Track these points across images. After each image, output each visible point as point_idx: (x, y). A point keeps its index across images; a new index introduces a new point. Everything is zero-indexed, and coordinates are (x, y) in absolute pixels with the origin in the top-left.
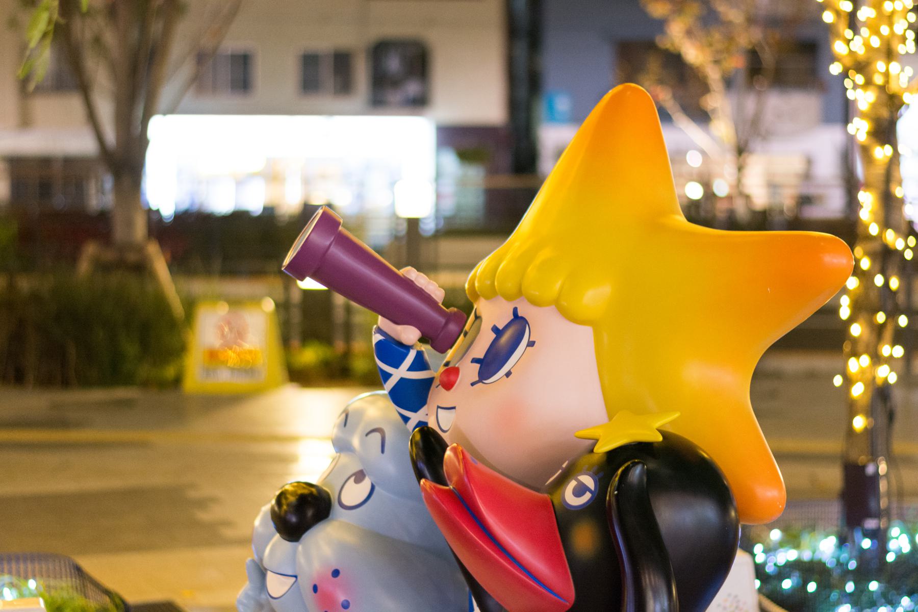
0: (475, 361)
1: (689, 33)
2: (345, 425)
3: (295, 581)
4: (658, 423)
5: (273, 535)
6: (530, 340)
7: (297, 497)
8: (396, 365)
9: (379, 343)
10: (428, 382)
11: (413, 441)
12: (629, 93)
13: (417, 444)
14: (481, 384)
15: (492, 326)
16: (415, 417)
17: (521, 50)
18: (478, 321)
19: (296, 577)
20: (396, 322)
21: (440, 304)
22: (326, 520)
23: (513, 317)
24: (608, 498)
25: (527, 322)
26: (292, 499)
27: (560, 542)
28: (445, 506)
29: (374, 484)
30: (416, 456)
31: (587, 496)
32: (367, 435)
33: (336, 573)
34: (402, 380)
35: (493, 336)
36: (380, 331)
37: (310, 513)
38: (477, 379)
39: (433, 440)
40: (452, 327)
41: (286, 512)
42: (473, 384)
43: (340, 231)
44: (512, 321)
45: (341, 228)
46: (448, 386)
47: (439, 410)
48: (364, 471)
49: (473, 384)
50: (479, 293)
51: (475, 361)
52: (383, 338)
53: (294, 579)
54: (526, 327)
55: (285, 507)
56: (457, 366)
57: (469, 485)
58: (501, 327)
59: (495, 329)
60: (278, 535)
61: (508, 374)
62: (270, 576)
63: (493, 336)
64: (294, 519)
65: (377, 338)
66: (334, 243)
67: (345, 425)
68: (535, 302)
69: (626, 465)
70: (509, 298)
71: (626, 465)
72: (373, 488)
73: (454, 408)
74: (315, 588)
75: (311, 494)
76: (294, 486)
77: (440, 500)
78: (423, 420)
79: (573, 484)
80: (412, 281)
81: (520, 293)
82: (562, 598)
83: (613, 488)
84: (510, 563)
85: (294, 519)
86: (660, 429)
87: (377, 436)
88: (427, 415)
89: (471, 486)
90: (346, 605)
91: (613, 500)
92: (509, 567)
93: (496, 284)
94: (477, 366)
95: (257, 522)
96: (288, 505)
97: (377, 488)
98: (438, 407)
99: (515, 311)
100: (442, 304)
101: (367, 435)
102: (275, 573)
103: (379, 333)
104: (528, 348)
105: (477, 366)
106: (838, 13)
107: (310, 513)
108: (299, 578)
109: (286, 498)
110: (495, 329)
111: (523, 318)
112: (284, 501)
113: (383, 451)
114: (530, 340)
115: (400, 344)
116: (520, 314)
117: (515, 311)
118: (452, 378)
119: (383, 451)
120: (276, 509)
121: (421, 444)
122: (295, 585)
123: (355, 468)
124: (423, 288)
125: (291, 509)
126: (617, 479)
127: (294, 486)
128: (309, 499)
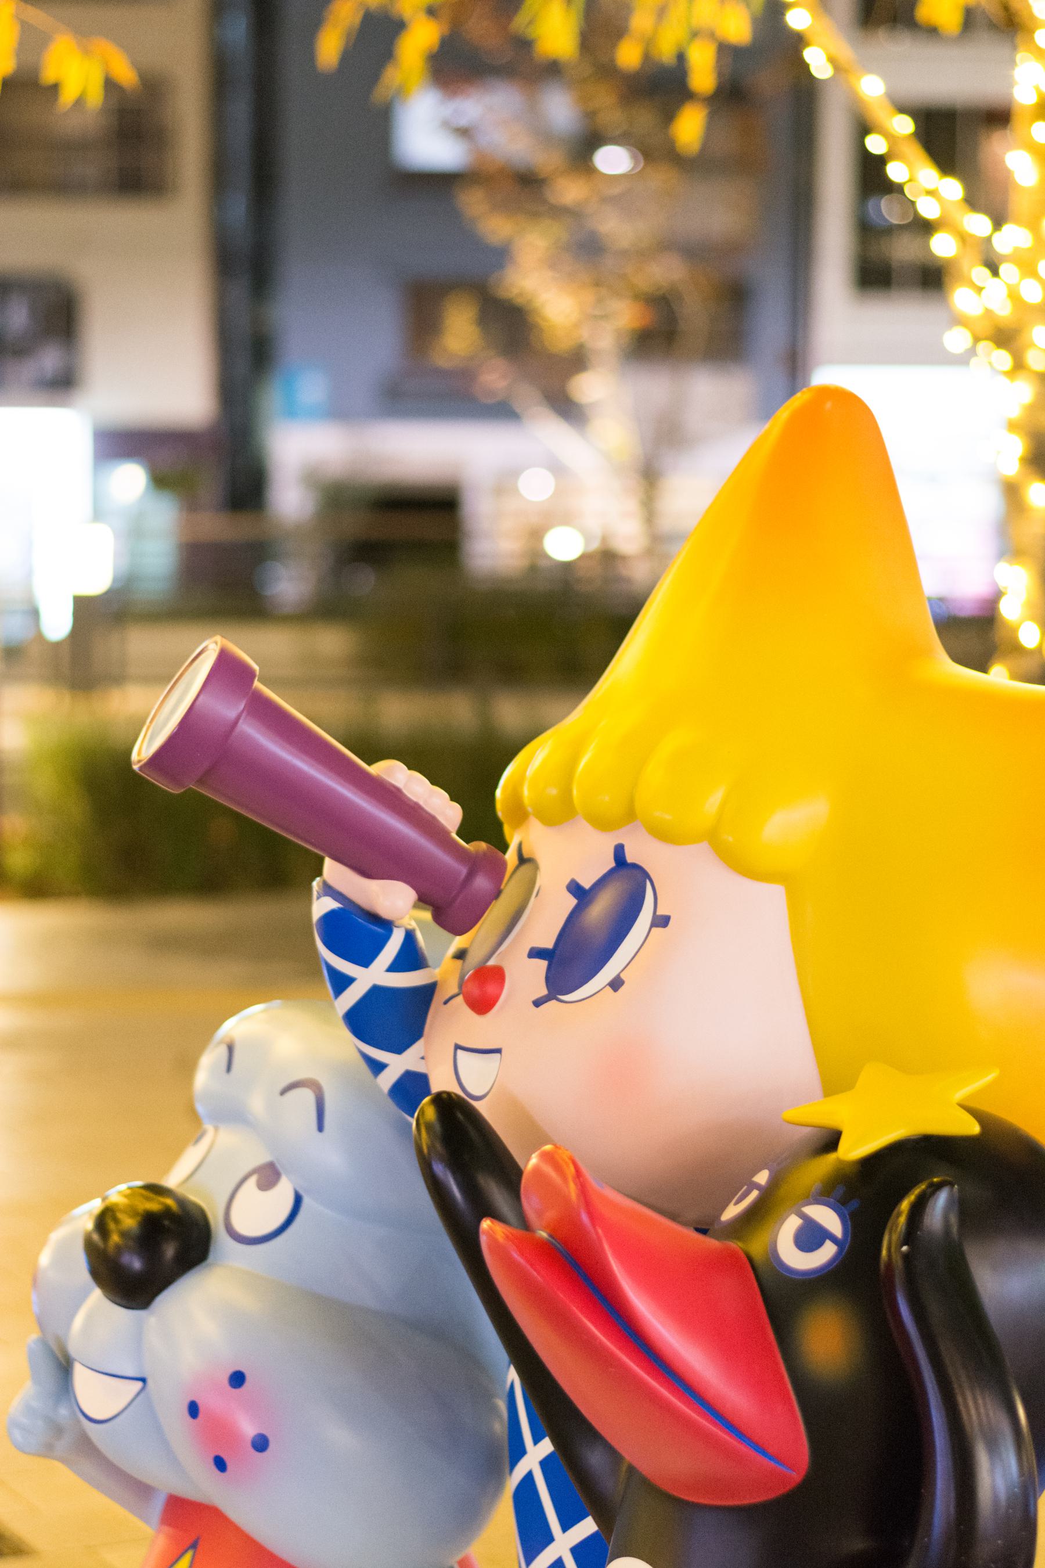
0: (536, 953)
1: (552, 263)
2: (229, 1068)
3: (143, 1389)
4: (961, 1094)
5: (85, 1294)
6: (659, 913)
7: (139, 1218)
8: (365, 960)
9: (329, 918)
10: (425, 994)
11: (421, 1121)
12: (828, 405)
13: (429, 1127)
14: (554, 1002)
15: (567, 881)
16: (397, 1065)
17: (239, 291)
18: (525, 868)
19: (143, 1380)
20: (367, 873)
21: (454, 836)
22: (204, 1264)
23: (613, 864)
24: (884, 1252)
25: (646, 875)
26: (129, 1223)
27: (775, 1344)
28: (538, 1273)
29: (301, 1192)
30: (428, 1148)
31: (827, 1252)
32: (283, 1092)
33: (237, 1379)
34: (376, 992)
35: (572, 902)
36: (329, 890)
37: (170, 1251)
38: (544, 991)
39: (460, 1116)
40: (481, 883)
41: (118, 1248)
42: (537, 1003)
43: (255, 688)
44: (611, 873)
45: (257, 684)
46: (482, 1005)
47: (459, 1052)
48: (278, 1166)
49: (537, 1003)
50: (529, 809)
51: (536, 953)
52: (340, 905)
53: (139, 1385)
54: (645, 884)
55: (115, 1238)
56: (491, 963)
57: (592, 1231)
58: (587, 884)
59: (575, 888)
60: (97, 1294)
61: (616, 984)
62: (80, 1374)
63: (572, 902)
64: (136, 1264)
65: (328, 904)
66: (244, 715)
67: (229, 1068)
68: (663, 835)
69: (917, 1191)
70: (602, 823)
71: (917, 1191)
72: (298, 1200)
73: (498, 1051)
74: (193, 1409)
75: (167, 1212)
76: (126, 1196)
77: (528, 1261)
78: (419, 1068)
79: (792, 1224)
80: (399, 790)
81: (630, 816)
82: (782, 1462)
83: (895, 1237)
84: (675, 1391)
85: (136, 1264)
86: (966, 1103)
87: (307, 1096)
88: (423, 1058)
89: (597, 1233)
90: (261, 1444)
91: (898, 1263)
92: (679, 1404)
93: (575, 792)
94: (542, 964)
95: (45, 1259)
96: (124, 1234)
97: (307, 1201)
98: (458, 1047)
99: (619, 852)
100: (458, 834)
101: (283, 1092)
102: (92, 1369)
103: (326, 894)
104: (654, 929)
105: (542, 964)
106: (964, 238)
107: (170, 1251)
108: (150, 1382)
109: (116, 1221)
110: (575, 888)
111: (636, 867)
112: (112, 1226)
113: (320, 1128)
114: (659, 913)
115: (375, 918)
116: (630, 858)
117: (619, 852)
118: (491, 989)
119: (320, 1128)
120: (96, 1237)
121: (438, 1128)
122: (142, 1395)
123: (262, 1158)
124: (421, 803)
125: (131, 1243)
126: (902, 1220)
127: (126, 1196)
128: (166, 1223)
